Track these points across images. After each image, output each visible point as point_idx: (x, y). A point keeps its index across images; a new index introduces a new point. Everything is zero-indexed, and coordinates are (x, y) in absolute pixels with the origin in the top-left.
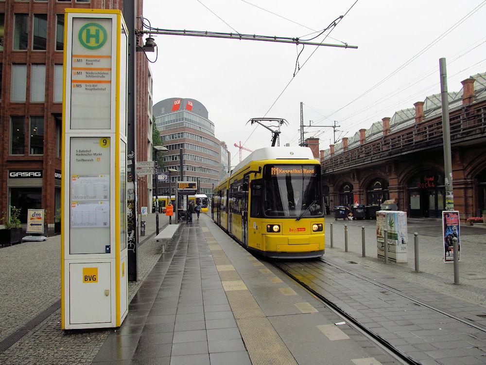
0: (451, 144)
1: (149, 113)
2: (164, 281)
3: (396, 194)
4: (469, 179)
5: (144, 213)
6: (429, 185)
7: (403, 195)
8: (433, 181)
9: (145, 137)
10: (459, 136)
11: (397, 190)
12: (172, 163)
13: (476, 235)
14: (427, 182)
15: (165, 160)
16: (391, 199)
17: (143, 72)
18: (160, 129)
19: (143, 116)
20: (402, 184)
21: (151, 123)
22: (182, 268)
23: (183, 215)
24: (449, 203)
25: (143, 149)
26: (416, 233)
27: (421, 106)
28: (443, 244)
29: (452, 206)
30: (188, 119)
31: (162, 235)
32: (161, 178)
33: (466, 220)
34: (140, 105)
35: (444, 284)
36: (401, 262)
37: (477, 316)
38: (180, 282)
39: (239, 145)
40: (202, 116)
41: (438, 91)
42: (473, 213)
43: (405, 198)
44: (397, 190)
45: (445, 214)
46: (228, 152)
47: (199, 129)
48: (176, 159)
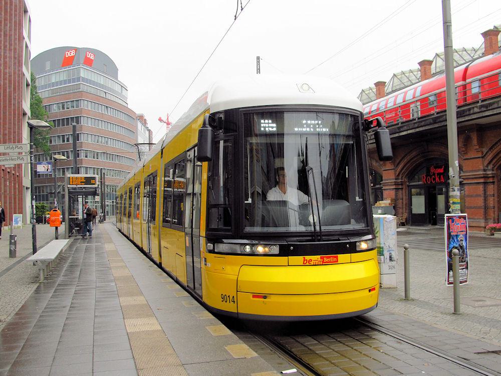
0: (458, 123)
1: (24, 70)
2: (39, 321)
3: (393, 193)
4: (489, 170)
5: (17, 223)
6: (437, 179)
7: (402, 194)
8: (442, 173)
9: (19, 107)
10: (476, 110)
11: (394, 187)
12: (61, 147)
13: (496, 248)
14: (434, 174)
15: (51, 142)
16: (386, 199)
17: (16, 6)
18: (43, 94)
19: (15, 73)
20: (400, 177)
21: (28, 85)
22: (67, 302)
23: (78, 225)
24: (454, 203)
25: (14, 124)
26: (407, 245)
27: (427, 66)
28: (445, 259)
29: (458, 207)
30: (90, 80)
31: (41, 255)
32: (41, 169)
33: (485, 227)
34: (10, 57)
35: (440, 315)
36: (388, 286)
37: (475, 353)
38: (62, 321)
39: (165, 119)
40: (108, 75)
41: (441, 49)
42: (494, 220)
43: (404, 197)
44: (394, 187)
45: (449, 218)
46: (149, 131)
47: (103, 95)
48: (68, 140)
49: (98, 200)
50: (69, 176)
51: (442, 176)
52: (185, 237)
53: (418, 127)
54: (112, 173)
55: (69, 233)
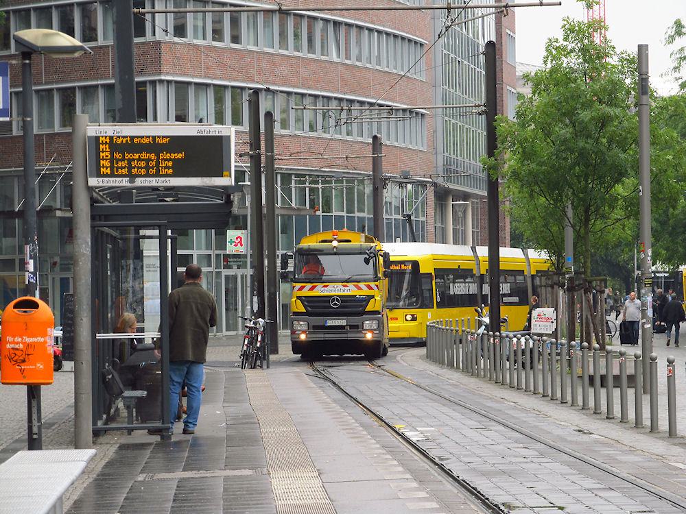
49: (241, 250)
54: (308, 116)
55: (96, 417)
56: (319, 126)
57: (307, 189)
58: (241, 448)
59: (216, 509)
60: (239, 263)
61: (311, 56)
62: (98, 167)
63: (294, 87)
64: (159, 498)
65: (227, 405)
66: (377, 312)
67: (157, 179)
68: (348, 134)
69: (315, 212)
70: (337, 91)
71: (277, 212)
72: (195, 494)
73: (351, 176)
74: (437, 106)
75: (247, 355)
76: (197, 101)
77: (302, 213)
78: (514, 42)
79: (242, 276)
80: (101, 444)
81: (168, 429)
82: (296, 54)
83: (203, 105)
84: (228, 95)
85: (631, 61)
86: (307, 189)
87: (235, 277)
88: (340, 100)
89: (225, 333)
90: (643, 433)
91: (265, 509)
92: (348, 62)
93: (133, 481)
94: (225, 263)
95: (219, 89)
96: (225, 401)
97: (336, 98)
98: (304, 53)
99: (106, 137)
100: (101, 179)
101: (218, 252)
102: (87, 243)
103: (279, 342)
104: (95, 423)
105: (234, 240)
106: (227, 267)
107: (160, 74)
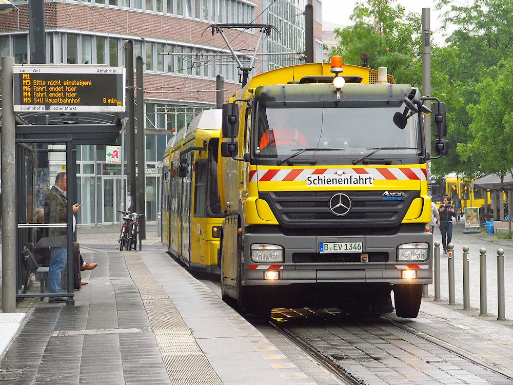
49: (117, 160)
50: (17, 69)
51: (215, 29)
52: (419, 336)
53: (302, 340)
54: (167, 60)
55: (18, 287)
56: (176, 68)
57: (166, 115)
58: (129, 312)
59: (116, 359)
60: (114, 171)
61: (169, 15)
62: (22, 97)
63: (156, 38)
64: (71, 350)
65: (114, 278)
66: (420, 227)
67: (67, 106)
68: (197, 74)
69: (172, 132)
70: (189, 42)
71: (145, 132)
72: (99, 347)
73: (201, 106)
74: (263, 53)
75: (124, 240)
76: (83, 48)
77: (163, 133)
78: (321, 5)
79: (117, 180)
80: (21, 308)
81: (72, 297)
82: (159, 13)
83: (88, 51)
84: (107, 44)
85: (416, 21)
86: (166, 115)
87: (111, 181)
88: (191, 48)
89: (104, 223)
90: (429, 301)
91: (154, 359)
92: (197, 19)
93: (49, 337)
94: (104, 171)
95: (101, 39)
96: (111, 275)
97: (188, 47)
98: (164, 13)
99: (27, 74)
100: (23, 106)
101: (99, 162)
102: (13, 155)
103: (146, 231)
104: (17, 292)
105: (112, 153)
106: (105, 173)
107: (56, 27)
